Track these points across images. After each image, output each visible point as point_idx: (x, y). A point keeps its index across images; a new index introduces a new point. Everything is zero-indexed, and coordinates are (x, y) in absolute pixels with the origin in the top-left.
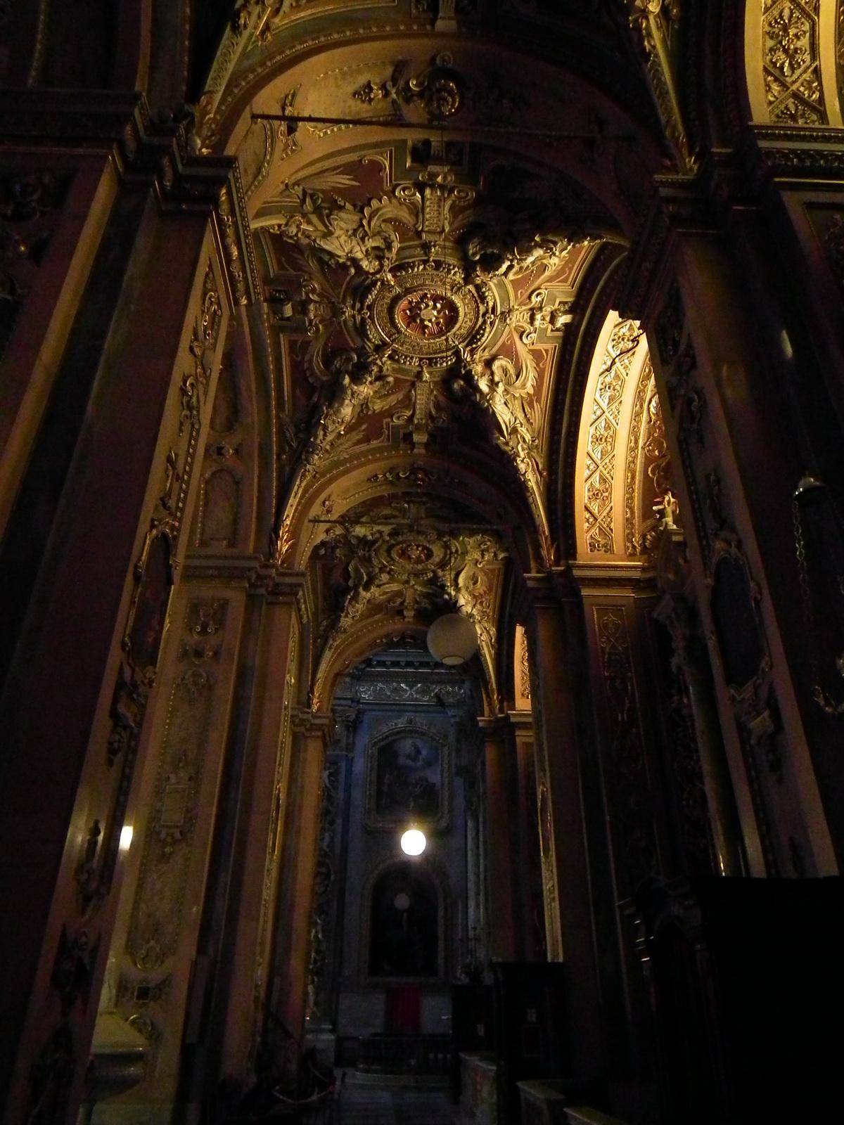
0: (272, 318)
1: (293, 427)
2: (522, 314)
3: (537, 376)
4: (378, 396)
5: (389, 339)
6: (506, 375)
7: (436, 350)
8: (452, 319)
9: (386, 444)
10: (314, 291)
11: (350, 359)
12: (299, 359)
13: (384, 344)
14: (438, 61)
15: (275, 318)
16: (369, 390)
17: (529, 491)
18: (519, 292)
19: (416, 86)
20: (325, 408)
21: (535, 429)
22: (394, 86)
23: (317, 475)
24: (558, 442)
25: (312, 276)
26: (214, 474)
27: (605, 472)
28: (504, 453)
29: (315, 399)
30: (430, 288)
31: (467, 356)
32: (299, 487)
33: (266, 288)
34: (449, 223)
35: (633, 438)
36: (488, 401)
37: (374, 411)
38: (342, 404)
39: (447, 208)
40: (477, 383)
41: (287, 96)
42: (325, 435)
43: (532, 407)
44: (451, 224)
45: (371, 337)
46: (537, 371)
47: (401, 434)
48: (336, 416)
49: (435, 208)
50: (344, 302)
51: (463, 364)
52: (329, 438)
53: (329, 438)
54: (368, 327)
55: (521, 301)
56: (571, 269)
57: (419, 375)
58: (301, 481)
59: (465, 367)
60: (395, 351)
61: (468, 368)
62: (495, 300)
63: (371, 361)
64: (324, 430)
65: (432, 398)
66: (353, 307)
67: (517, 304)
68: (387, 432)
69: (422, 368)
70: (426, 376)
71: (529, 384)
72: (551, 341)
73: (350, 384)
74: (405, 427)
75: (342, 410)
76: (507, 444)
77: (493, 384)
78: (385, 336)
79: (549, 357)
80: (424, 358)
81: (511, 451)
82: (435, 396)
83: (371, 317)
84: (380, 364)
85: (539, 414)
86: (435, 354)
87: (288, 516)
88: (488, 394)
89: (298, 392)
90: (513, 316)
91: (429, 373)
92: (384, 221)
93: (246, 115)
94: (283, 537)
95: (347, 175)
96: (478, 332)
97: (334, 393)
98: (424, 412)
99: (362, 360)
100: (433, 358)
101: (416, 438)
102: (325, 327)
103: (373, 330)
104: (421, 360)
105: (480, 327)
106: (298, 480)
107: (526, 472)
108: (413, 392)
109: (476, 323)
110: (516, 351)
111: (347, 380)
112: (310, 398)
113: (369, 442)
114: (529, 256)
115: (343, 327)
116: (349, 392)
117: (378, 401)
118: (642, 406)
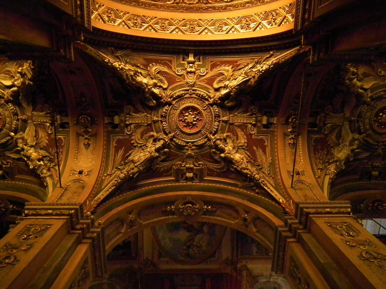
0: (196, 181)
2: (189, 77)
3: (224, 65)
4: (237, 141)
5: (204, 135)
6: (222, 81)
8: (194, 109)
10: (181, 165)
11: (214, 153)
12: (216, 173)
14: (283, 123)
15: (196, 180)
16: (230, 145)
17: (279, 62)
18: (177, 80)
21: (251, 62)
22: (290, 136)
24: (256, 48)
25: (173, 164)
27: (209, 24)
28: (259, 77)
29: (232, 170)
30: (176, 119)
31: (211, 101)
33: (181, 182)
34: (143, 113)
35: (247, 5)
36: (232, 89)
37: (245, 142)
38: (233, 159)
39: (136, 115)
40: (223, 95)
42: (247, 169)
43: (239, 65)
44: (143, 113)
45: (201, 143)
46: (221, 65)
49: (136, 119)
52: (249, 167)
53: (249, 167)
54: (197, 144)
55: (182, 79)
56: (162, 60)
57: (226, 122)
58: (266, 186)
59: (216, 101)
60: (211, 133)
61: (217, 99)
62: (181, 90)
64: (244, 169)
65: (240, 115)
67: (184, 80)
68: (261, 137)
69: (220, 120)
70: (225, 118)
71: (227, 68)
72: (205, 61)
74: (259, 127)
75: (236, 159)
76: (254, 77)
77: (225, 87)
79: (213, 60)
80: (215, 120)
81: (258, 75)
82: (239, 113)
83: (192, 143)
84: (215, 140)
85: (242, 60)
88: (229, 89)
89: (230, 176)
90: (189, 82)
91: (223, 117)
92: (141, 138)
94: (286, 206)
95: (119, 152)
96: (199, 96)
97: (229, 161)
98: (249, 119)
101: (265, 122)
102: (200, 161)
103: (199, 142)
104: (215, 121)
105: (197, 95)
107: (268, 65)
108: (236, 124)
109: (195, 98)
110: (212, 77)
111: (222, 155)
112: (232, 172)
114: (142, 82)
115: (199, 154)
116: (227, 155)
118: (230, 6)
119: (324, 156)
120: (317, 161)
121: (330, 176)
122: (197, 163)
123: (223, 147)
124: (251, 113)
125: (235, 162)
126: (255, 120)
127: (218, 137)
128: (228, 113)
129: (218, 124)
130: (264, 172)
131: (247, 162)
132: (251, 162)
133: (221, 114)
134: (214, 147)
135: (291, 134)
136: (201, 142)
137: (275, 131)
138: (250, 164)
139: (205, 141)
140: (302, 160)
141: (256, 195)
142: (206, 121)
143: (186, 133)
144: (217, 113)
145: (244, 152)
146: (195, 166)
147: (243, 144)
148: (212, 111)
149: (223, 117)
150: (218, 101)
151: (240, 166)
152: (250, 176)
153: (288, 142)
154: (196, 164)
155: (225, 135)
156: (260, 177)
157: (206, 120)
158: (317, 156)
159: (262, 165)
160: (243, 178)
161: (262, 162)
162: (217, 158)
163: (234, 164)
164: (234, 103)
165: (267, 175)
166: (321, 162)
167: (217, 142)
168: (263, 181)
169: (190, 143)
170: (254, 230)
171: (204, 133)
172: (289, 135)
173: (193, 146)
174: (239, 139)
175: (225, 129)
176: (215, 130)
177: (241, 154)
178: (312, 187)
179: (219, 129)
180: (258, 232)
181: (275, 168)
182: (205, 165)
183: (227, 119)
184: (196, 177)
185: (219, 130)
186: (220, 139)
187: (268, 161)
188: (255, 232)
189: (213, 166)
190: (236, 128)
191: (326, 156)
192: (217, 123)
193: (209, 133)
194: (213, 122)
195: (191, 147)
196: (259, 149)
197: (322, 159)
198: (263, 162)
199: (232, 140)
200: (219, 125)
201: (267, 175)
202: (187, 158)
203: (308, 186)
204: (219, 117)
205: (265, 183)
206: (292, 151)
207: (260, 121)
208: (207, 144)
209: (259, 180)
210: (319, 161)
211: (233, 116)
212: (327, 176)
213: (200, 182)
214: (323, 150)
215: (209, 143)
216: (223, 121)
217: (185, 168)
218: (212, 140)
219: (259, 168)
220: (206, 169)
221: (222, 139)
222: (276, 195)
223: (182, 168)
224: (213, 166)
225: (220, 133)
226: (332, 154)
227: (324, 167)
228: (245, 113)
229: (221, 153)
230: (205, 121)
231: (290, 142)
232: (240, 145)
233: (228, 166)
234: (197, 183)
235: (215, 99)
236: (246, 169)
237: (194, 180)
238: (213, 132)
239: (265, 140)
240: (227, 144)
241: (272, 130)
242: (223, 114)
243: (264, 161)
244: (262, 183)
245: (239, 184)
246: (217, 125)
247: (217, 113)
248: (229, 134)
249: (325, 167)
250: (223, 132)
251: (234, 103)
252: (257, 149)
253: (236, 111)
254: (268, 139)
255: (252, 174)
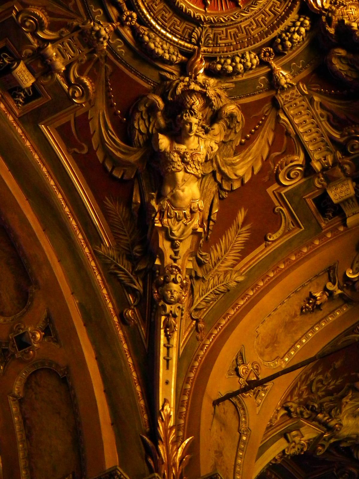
0: (13, 105)
1: (125, 262)
4: (232, 152)
5: (190, 42)
7: (271, 21)
9: (297, 231)
10: (40, 26)
11: (152, 109)
12: (85, 152)
13: (189, 54)
15: (17, 102)
16: (208, 143)
19: (354, 273)
20: (153, 203)
22: (334, 284)
23: (201, 325)
26: (27, 385)
29: (137, 198)
32: (168, 348)
37: (242, 179)
38: (174, 183)
41: (237, 360)
45: (161, 52)
47: (312, 205)
48: (177, 208)
50: (90, 17)
51: (324, 18)
52: (184, 248)
53: (184, 248)
54: (147, 38)
59: (329, 20)
60: (211, 59)
61: (335, 19)
63: (183, 91)
64: (168, 238)
65: (319, 111)
66: (109, 19)
68: (284, 210)
73: (171, 144)
74: (309, 186)
78: (182, 43)
82: (322, 106)
83: (142, 20)
84: (198, 88)
86: (273, 28)
87: (166, 401)
89: (109, 203)
91: (284, 67)
93: (206, 405)
94: (167, 438)
98: (321, 145)
99: (170, 99)
100: (274, 39)
102: (93, 77)
103: (158, 39)
104: (258, 51)
106: (162, 336)
108: (283, 117)
111: (164, 142)
112: (129, 202)
113: (266, 240)
115: (117, 62)
116: (176, 157)
117: (236, 159)
119: (323, 389)
120: (301, 384)
121: (288, 448)
122: (81, 72)
123: (191, 130)
124: (342, 140)
125: (169, 197)
126: (328, 163)
127: (211, 93)
128: (304, 74)
129: (252, 65)
130: (195, 293)
131: (194, 232)
132: (200, 238)
133: (290, 56)
134: (170, 99)
135: (341, 284)
136: (163, 49)
137: (324, 235)
138: (192, 242)
139: (175, 58)
140: (287, 359)
141: (116, 319)
142: (241, 22)
143: (181, 8)
144: (289, 43)
145: (212, 196)
146: (66, 75)
147: (233, 177)
148: (288, 22)
149: (285, 67)
150: (330, 26)
151: (168, 217)
152: (161, 268)
153: (312, 290)
154: (74, 73)
155: (232, 108)
156: (179, 300)
157: (246, 19)
158: (312, 377)
159: (207, 272)
160: (137, 248)
161: (215, 264)
162: (141, 128)
163: (160, 197)
164: (346, 75)
165: (194, 307)
166: (305, 396)
167: (194, 98)
168: (175, 316)
169: (134, 15)
170: (17, 388)
171: (199, 40)
172: (335, 279)
173: (133, 29)
174: (242, 155)
175: (247, 96)
176: (231, 68)
177: (203, 196)
178: (244, 443)
179: (240, 78)
180: (21, 402)
181: (221, 312)
182: (90, 102)
183: (286, 83)
184: (27, 100)
185: (235, 79)
186: (208, 102)
187: (228, 276)
188: (14, 396)
189: (103, 130)
190: (269, 125)
191: (323, 393)
192: (255, 62)
193: (208, 55)
194: (250, 47)
195: (123, 24)
196: (244, 229)
197: (311, 392)
198: (216, 268)
199: (226, 136)
200: (251, 69)
201: (194, 307)
202: (76, 35)
203: (239, 430)
204: (279, 54)
205: (175, 326)
206: (296, 315)
207: (330, 180)
208: (167, 68)
209: (170, 303)
210: (303, 392)
211: (303, 94)
212: (283, 440)
213: (19, 118)
214: (336, 374)
215: (172, 74)
216: (271, 75)
217: (36, 45)
218: (190, 77)
219: (196, 272)
220: (79, 114)
221: (211, 106)
222: (167, 383)
223: (29, 36)
224: (103, 130)
225: (226, 89)
226: (338, 404)
227: (297, 413)
228: (331, 124)
229: (165, 132)
230: (239, 20)
231: (318, 295)
232: (225, 170)
233: (137, 176)
234: (11, 112)
235: (333, 12)
236: (172, 241)
237: (14, 96)
238: (219, 66)
239: (282, 227)
240: (207, 132)
241: (320, 226)
242: (293, 60)
243: (222, 267)
244: (168, 316)
245: (105, 246)
246: (249, 64)
247: (289, 43)
248: (240, 117)
249: (300, 416)
250: (233, 95)
251: (346, 75)
252: (244, 224)
253: (325, 94)
254: (290, 231)
255: (172, 273)
